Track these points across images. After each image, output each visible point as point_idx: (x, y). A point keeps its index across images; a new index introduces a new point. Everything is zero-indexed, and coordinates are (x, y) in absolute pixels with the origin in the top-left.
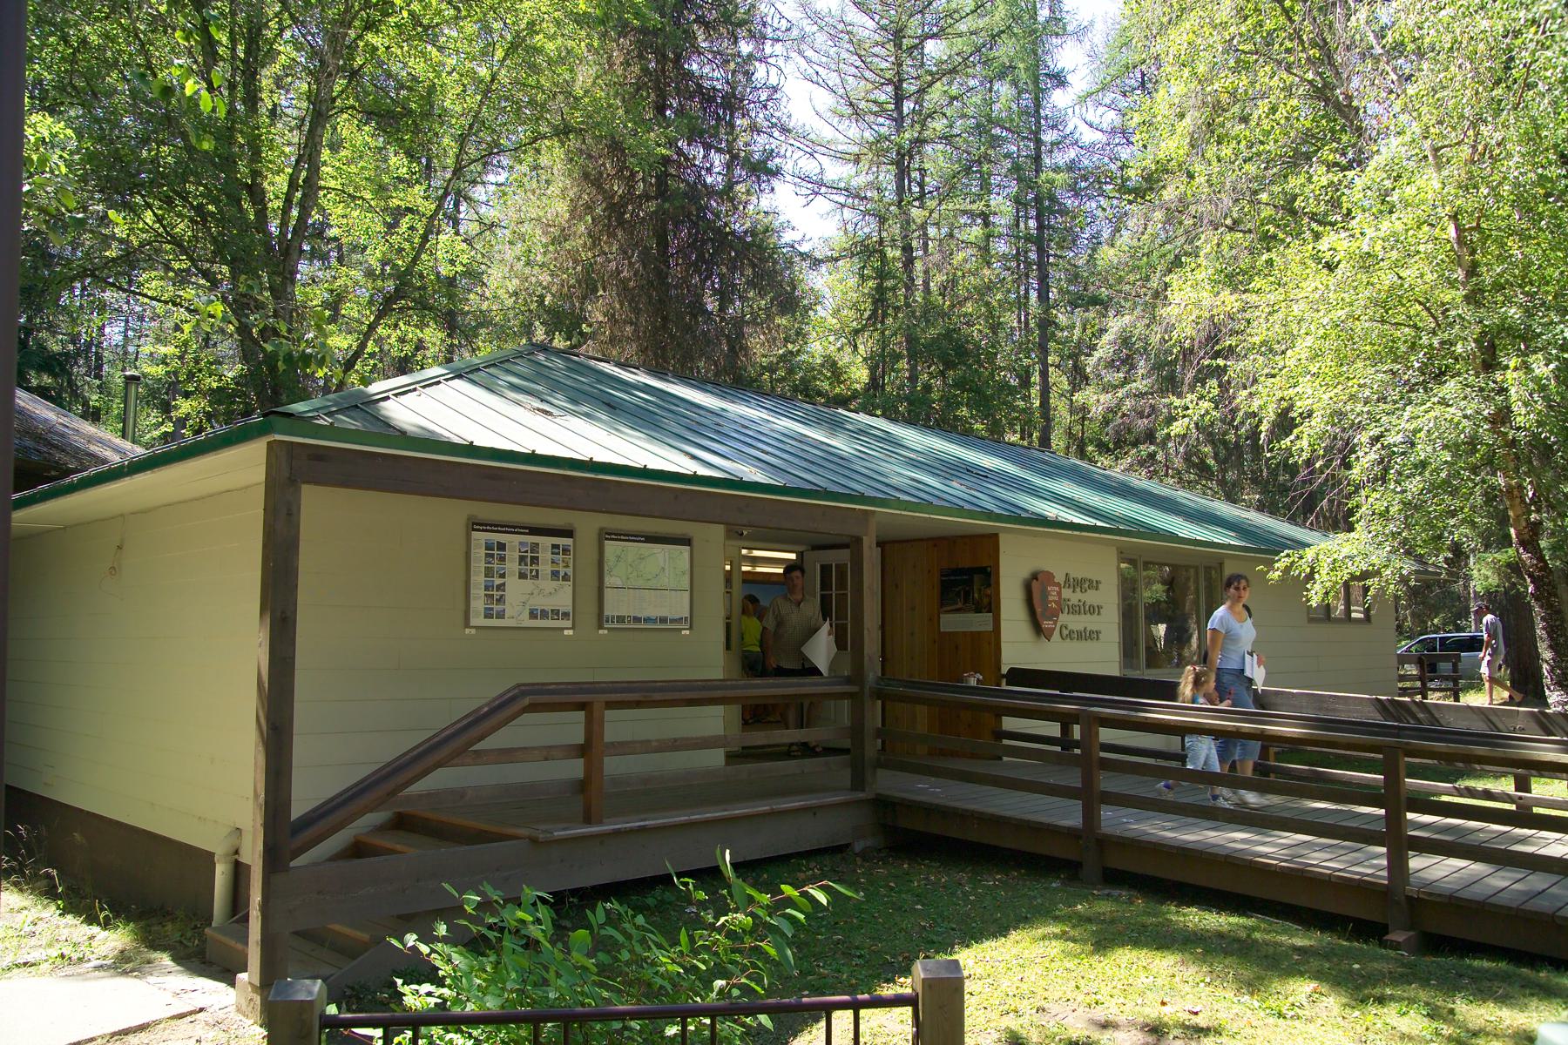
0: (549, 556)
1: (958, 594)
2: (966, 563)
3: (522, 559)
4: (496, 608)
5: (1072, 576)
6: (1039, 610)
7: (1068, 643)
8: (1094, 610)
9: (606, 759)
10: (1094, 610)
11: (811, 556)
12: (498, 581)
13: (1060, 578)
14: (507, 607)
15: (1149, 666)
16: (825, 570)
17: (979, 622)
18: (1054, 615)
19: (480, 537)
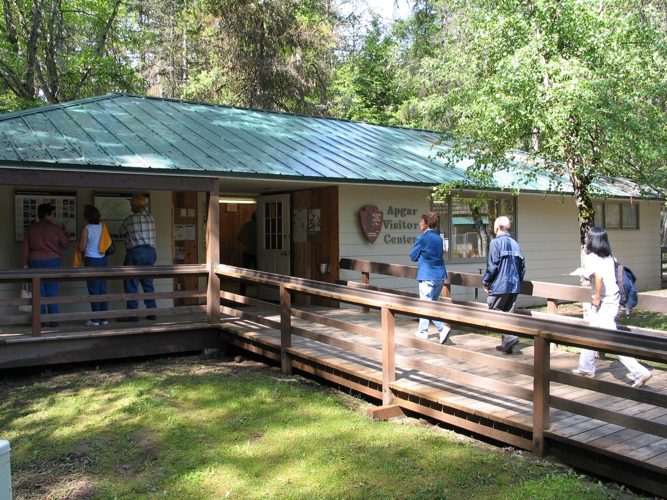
6: (365, 227)
7: (391, 245)
19: (20, 198)
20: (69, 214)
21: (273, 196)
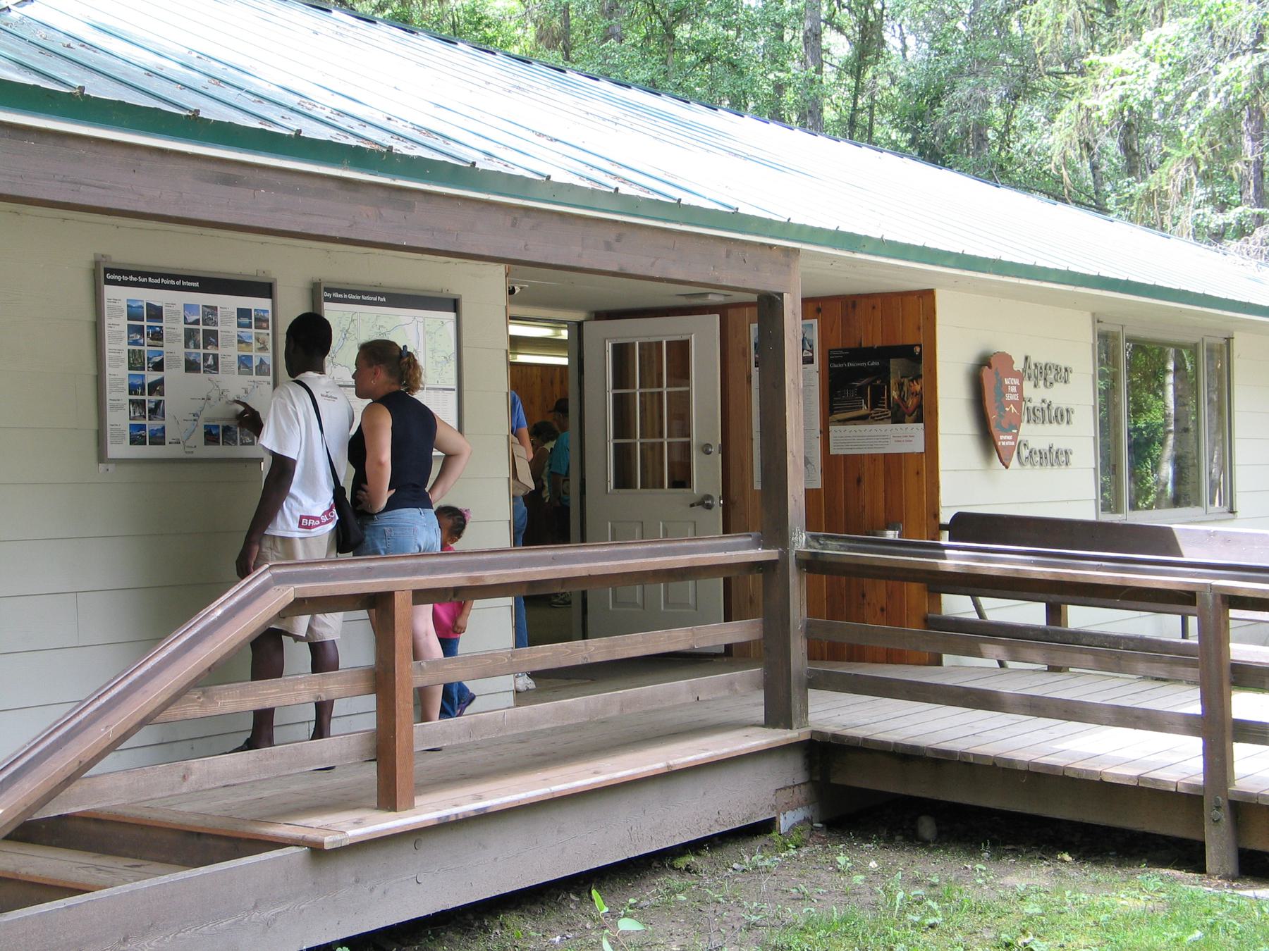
0: (234, 330)
1: (861, 392)
2: (875, 338)
3: (190, 336)
4: (151, 425)
5: (1033, 360)
6: (993, 417)
8: (1062, 416)
9: (1199, 712)
10: (1062, 416)
11: (594, 330)
12: (151, 377)
13: (1018, 365)
14: (168, 423)
15: (1134, 507)
16: (622, 352)
17: (903, 438)
18: (1013, 426)
19: (118, 297)
20: (256, 362)
21: (169, 213)
